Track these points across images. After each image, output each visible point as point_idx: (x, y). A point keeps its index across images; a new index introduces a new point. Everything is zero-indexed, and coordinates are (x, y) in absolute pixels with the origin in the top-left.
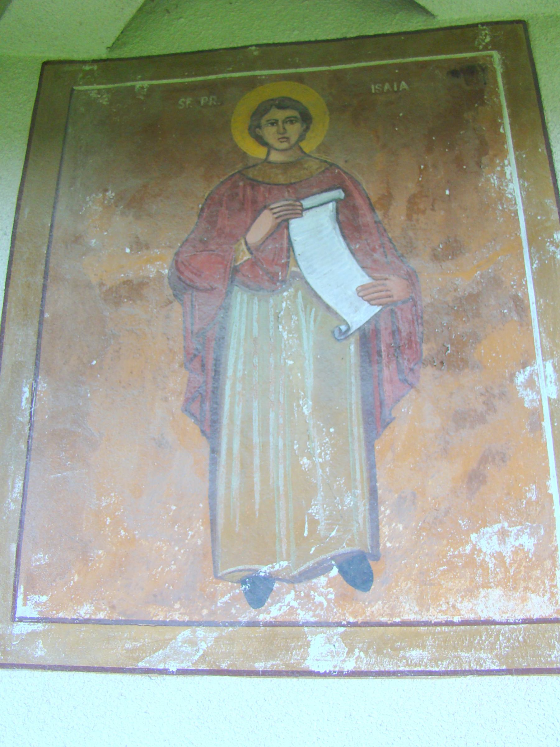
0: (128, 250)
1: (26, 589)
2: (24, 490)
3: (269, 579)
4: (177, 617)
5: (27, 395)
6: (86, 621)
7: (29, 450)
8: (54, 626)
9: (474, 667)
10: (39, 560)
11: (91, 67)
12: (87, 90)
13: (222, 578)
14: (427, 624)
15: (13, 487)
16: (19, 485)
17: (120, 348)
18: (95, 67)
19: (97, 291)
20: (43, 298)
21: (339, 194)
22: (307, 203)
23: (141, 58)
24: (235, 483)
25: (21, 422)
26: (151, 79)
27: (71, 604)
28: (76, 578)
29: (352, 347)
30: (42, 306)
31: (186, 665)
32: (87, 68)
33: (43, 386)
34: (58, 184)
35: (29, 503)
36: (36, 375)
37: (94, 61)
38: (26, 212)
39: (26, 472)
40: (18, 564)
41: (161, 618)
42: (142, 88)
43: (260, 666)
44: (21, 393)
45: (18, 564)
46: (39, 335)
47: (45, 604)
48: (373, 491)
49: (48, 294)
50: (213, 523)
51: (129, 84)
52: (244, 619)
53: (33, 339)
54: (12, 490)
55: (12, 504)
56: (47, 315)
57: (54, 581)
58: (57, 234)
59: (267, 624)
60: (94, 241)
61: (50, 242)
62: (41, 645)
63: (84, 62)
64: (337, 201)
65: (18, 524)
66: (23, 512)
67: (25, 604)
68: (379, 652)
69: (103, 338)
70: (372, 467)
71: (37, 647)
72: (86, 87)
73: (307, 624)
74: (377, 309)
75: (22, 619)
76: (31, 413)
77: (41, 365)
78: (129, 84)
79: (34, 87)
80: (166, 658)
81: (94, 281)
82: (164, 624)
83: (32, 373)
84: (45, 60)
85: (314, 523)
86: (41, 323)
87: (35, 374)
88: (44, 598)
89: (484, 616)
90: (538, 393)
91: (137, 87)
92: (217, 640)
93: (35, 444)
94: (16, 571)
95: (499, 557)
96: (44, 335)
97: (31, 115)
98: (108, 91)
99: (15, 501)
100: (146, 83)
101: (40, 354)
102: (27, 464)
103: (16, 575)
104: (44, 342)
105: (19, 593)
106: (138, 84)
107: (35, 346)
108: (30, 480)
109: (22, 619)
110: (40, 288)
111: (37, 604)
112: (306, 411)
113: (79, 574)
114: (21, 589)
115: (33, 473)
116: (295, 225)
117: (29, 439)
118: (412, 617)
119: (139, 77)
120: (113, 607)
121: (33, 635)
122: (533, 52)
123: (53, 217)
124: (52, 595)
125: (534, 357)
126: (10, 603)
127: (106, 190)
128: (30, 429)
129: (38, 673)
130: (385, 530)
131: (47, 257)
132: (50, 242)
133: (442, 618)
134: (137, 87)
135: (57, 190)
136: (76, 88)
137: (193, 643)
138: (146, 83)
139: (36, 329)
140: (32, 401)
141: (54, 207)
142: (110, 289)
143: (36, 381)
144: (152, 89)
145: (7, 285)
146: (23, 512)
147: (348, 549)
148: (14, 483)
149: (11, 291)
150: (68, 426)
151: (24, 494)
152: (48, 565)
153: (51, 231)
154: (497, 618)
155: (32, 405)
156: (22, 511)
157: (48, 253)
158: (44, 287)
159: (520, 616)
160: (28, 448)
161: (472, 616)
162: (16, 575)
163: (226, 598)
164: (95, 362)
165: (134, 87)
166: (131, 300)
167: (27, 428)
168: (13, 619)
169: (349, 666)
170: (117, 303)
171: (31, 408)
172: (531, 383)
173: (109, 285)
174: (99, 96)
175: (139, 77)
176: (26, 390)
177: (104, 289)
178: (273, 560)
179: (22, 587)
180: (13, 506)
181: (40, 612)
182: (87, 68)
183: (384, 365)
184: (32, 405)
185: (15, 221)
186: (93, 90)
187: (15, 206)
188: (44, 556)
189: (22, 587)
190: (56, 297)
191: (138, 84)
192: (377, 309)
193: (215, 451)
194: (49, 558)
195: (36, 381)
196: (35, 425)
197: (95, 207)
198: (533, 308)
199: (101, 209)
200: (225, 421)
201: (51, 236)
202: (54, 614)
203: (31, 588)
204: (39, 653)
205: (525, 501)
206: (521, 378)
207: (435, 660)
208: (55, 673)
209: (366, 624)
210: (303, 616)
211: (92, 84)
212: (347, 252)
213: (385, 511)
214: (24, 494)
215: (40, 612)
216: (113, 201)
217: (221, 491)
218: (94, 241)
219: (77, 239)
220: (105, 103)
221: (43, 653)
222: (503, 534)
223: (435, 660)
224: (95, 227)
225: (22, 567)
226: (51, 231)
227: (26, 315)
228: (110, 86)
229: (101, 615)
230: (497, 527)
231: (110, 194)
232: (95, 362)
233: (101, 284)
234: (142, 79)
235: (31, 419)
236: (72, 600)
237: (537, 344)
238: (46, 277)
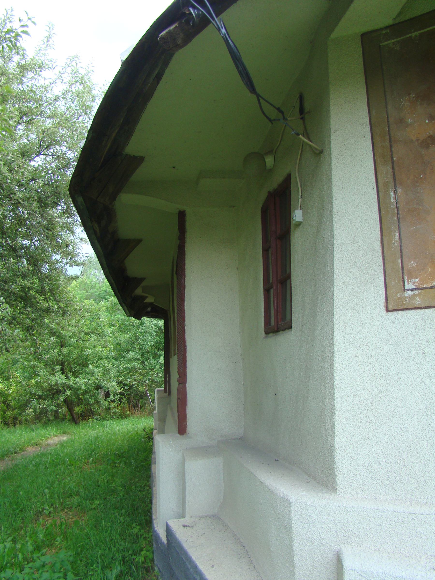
0: (427, 121)
1: (408, 278)
2: (399, 236)
5: (393, 196)
7: (398, 219)
8: (423, 291)
10: (412, 264)
11: (386, 31)
12: (387, 44)
15: (395, 236)
16: (397, 235)
17: (432, 168)
18: (388, 31)
19: (417, 143)
20: (391, 151)
23: (411, 19)
25: (392, 208)
26: (420, 30)
27: (429, 281)
28: (430, 270)
30: (392, 155)
32: (384, 32)
33: (399, 191)
34: (385, 96)
35: (403, 242)
36: (395, 187)
37: (387, 27)
38: (373, 112)
39: (399, 229)
40: (402, 268)
42: (416, 36)
44: (390, 195)
45: (402, 268)
46: (393, 168)
47: (418, 282)
49: (393, 149)
51: (408, 36)
53: (390, 171)
54: (394, 238)
55: (395, 243)
56: (395, 159)
57: (420, 272)
58: (391, 120)
60: (409, 120)
61: (388, 125)
62: (418, 299)
63: (382, 29)
65: (400, 251)
66: (401, 246)
67: (408, 284)
69: (423, 164)
71: (417, 300)
72: (386, 43)
75: (408, 290)
76: (396, 203)
77: (397, 181)
78: (408, 36)
79: (360, 49)
81: (414, 139)
83: (393, 186)
84: (361, 33)
86: (393, 163)
87: (395, 186)
88: (417, 280)
91: (413, 36)
93: (401, 216)
94: (402, 271)
96: (395, 167)
97: (363, 64)
98: (398, 42)
99: (396, 242)
100: (417, 33)
101: (395, 177)
102: (399, 226)
103: (403, 272)
104: (396, 171)
105: (405, 280)
106: (413, 34)
107: (392, 174)
108: (402, 232)
109: (408, 290)
110: (389, 147)
111: (414, 283)
113: (431, 268)
114: (406, 278)
115: (402, 229)
117: (397, 215)
119: (413, 30)
121: (414, 295)
122: (343, 561)
123: (387, 112)
124: (420, 278)
126: (402, 284)
127: (410, 94)
128: (397, 210)
129: (418, 311)
131: (389, 132)
132: (388, 125)
134: (413, 36)
135: (386, 99)
136: (381, 44)
138: (417, 33)
139: (391, 166)
140: (396, 198)
141: (386, 108)
142: (422, 142)
143: (396, 189)
144: (421, 35)
145: (373, 148)
148: (394, 234)
149: (375, 151)
150: (415, 206)
151: (400, 238)
152: (417, 266)
153: (388, 119)
155: (396, 199)
156: (400, 245)
157: (389, 130)
158: (391, 146)
160: (398, 219)
162: (403, 272)
164: (422, 176)
165: (411, 37)
166: (433, 145)
167: (396, 210)
168: (404, 290)
170: (427, 147)
171: (396, 201)
173: (421, 140)
174: (394, 46)
175: (413, 30)
176: (392, 194)
177: (420, 142)
179: (406, 277)
180: (396, 244)
181: (416, 286)
182: (384, 32)
184: (396, 199)
185: (369, 118)
186: (390, 43)
187: (367, 111)
188: (414, 263)
189: (406, 277)
190: (397, 150)
191: (413, 34)
194: (416, 263)
195: (396, 189)
196: (399, 208)
197: (406, 104)
199: (409, 104)
201: (388, 122)
202: (422, 286)
203: (410, 277)
204: (418, 302)
208: (426, 310)
211: (389, 40)
214: (400, 238)
215: (416, 286)
216: (414, 99)
218: (409, 120)
219: (401, 121)
220: (398, 49)
221: (420, 302)
224: (409, 113)
225: (404, 269)
226: (388, 119)
227: (385, 160)
228: (398, 39)
231: (412, 96)
232: (422, 176)
233: (418, 140)
234: (414, 31)
235: (397, 206)
236: (429, 279)
238: (390, 141)
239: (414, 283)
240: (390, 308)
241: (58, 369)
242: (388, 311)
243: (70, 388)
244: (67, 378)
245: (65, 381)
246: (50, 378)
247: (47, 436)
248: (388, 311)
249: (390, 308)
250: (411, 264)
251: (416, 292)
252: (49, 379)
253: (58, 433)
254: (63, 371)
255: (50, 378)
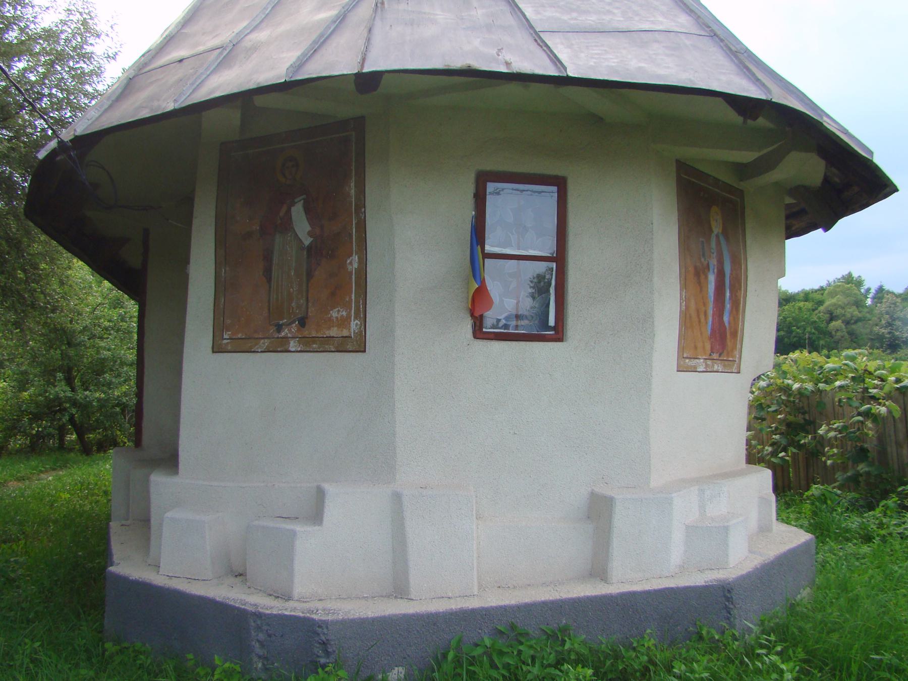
3: (282, 325)
4: (260, 336)
6: (241, 339)
9: (329, 350)
13: (271, 325)
14: (318, 337)
21: (304, 196)
22: (296, 200)
24: (275, 297)
29: (305, 253)
31: (263, 350)
41: (256, 337)
43: (279, 349)
48: (307, 298)
50: (269, 309)
52: (276, 336)
56: (227, 245)
59: (281, 338)
64: (304, 199)
66: (224, 308)
68: (306, 345)
70: (307, 291)
73: (290, 338)
74: (312, 239)
75: (225, 339)
80: (257, 348)
82: (257, 338)
85: (293, 308)
88: (230, 333)
89: (332, 335)
90: (352, 266)
92: (270, 343)
95: (337, 318)
109: (225, 339)
111: (228, 334)
112: (292, 274)
116: (293, 209)
118: (314, 335)
120: (246, 335)
125: (353, 254)
130: (309, 310)
133: (321, 336)
137: (264, 343)
140: (225, 273)
146: (224, 308)
147: (300, 316)
152: (570, 658)
154: (335, 336)
159: (341, 336)
161: (328, 335)
163: (272, 331)
169: (299, 349)
172: (351, 263)
178: (282, 319)
183: (606, 667)
192: (312, 239)
193: (270, 287)
198: (354, 236)
200: (273, 278)
203: (228, 330)
205: (584, 637)
206: (348, 261)
207: (319, 348)
209: (303, 337)
210: (289, 335)
212: (306, 219)
213: (310, 304)
217: (272, 299)
222: (339, 311)
223: (319, 348)
229: (243, 337)
230: (337, 309)
237: (354, 249)
239: (228, 334)
240: (215, 350)
241: (60, 377)
242: (213, 352)
243: (75, 403)
244: (73, 390)
245: (69, 394)
246: (49, 389)
247: (40, 468)
248: (213, 352)
249: (215, 350)
250: (228, 321)
251: (229, 341)
252: (46, 391)
253: (57, 466)
254: (69, 381)
255: (49, 389)
